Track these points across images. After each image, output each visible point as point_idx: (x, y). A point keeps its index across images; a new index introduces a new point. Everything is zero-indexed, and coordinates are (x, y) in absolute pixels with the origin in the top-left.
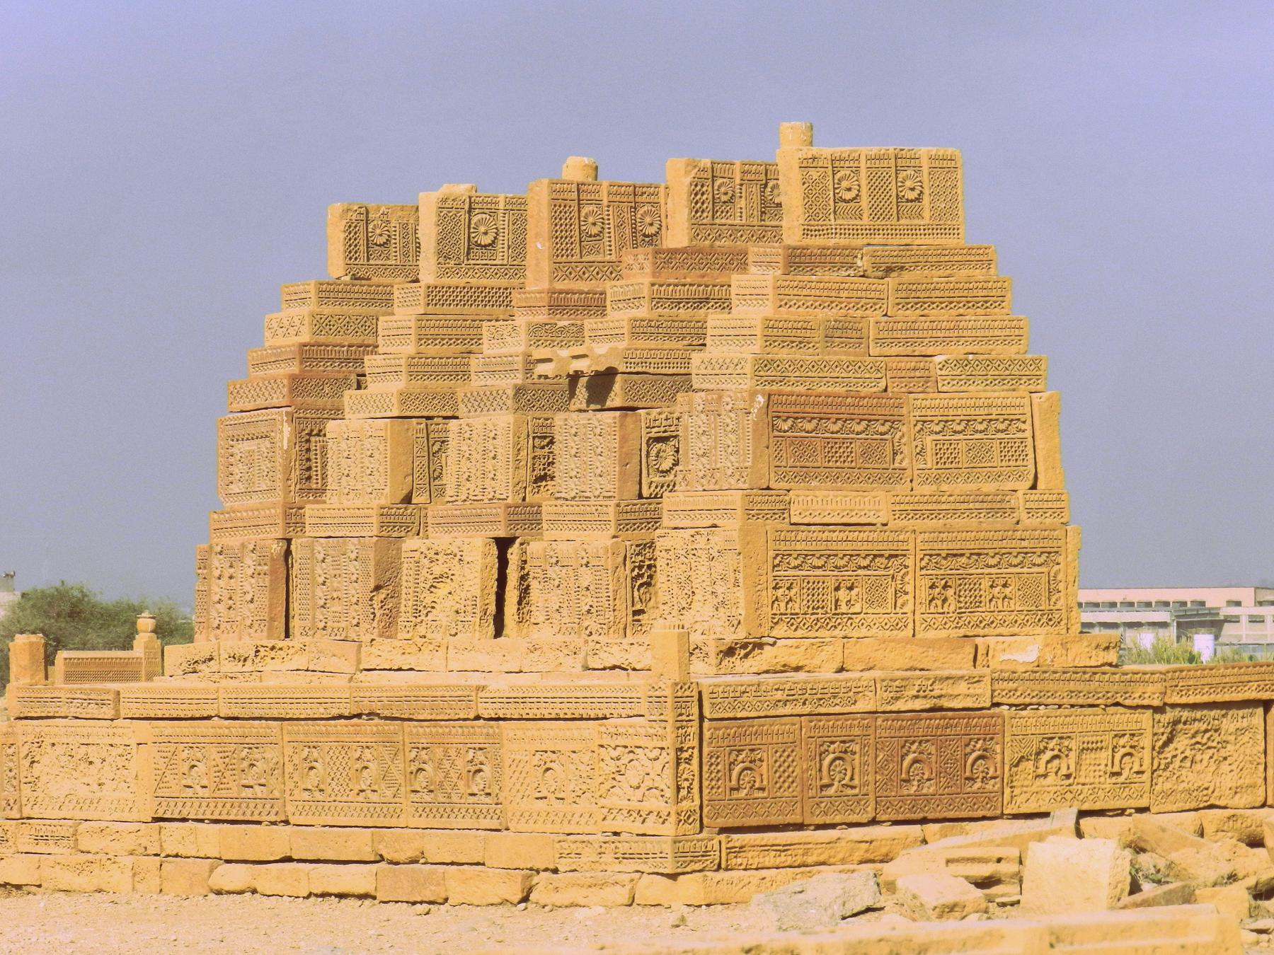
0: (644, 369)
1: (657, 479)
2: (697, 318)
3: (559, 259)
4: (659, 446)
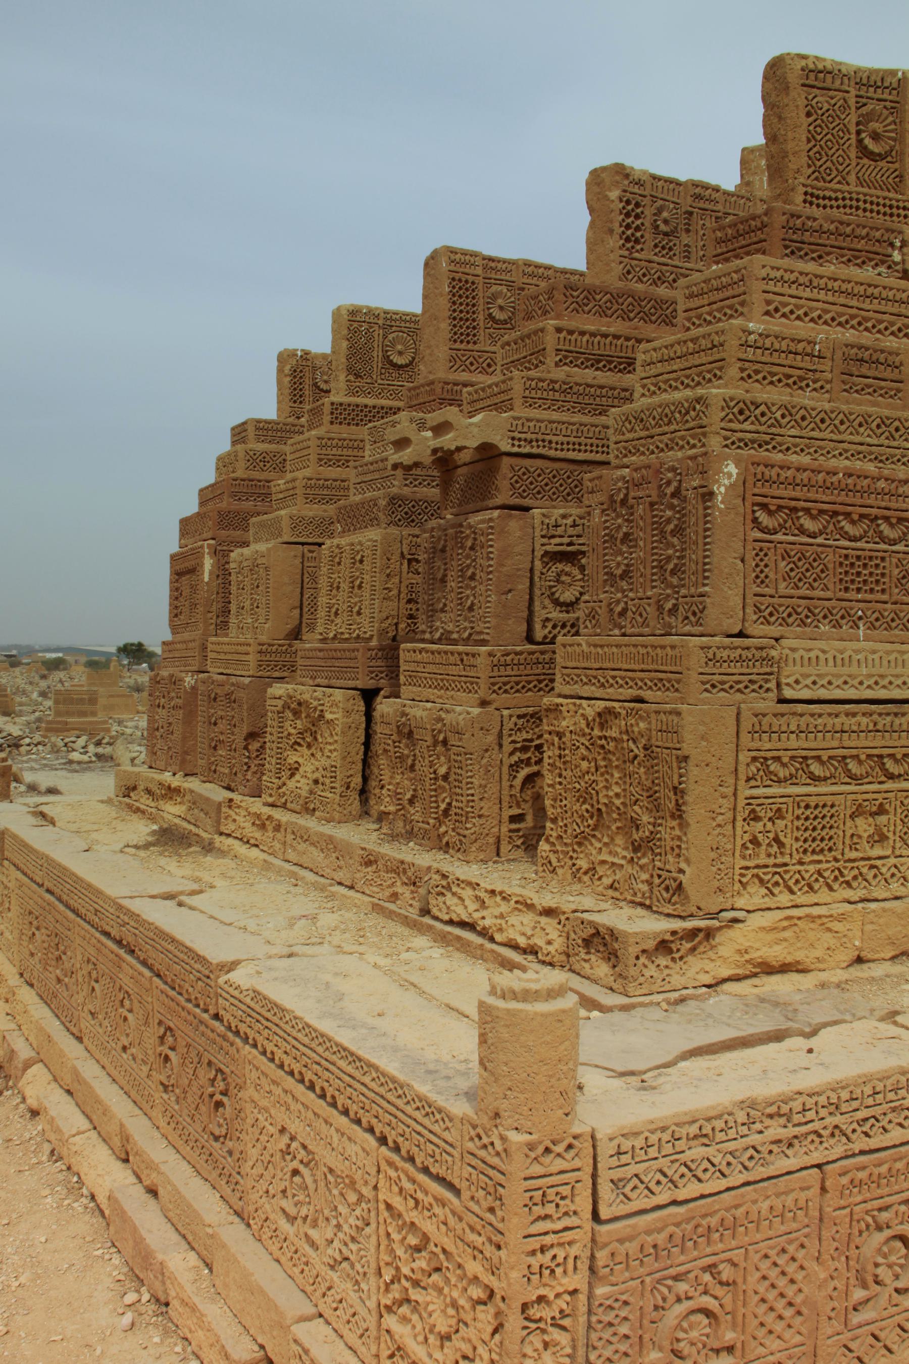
0: (541, 451)
1: (556, 615)
3: (457, 346)
4: (560, 566)
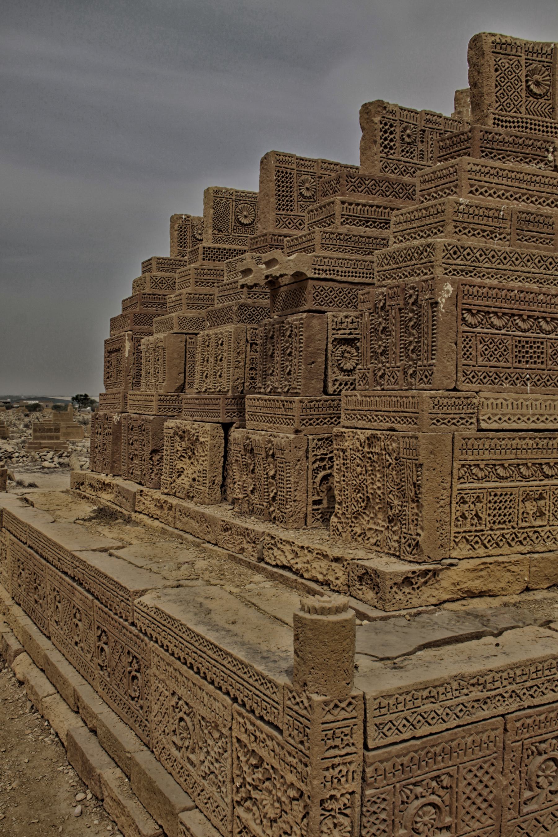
1: (341, 377)
2: (383, 236)
3: (281, 212)
